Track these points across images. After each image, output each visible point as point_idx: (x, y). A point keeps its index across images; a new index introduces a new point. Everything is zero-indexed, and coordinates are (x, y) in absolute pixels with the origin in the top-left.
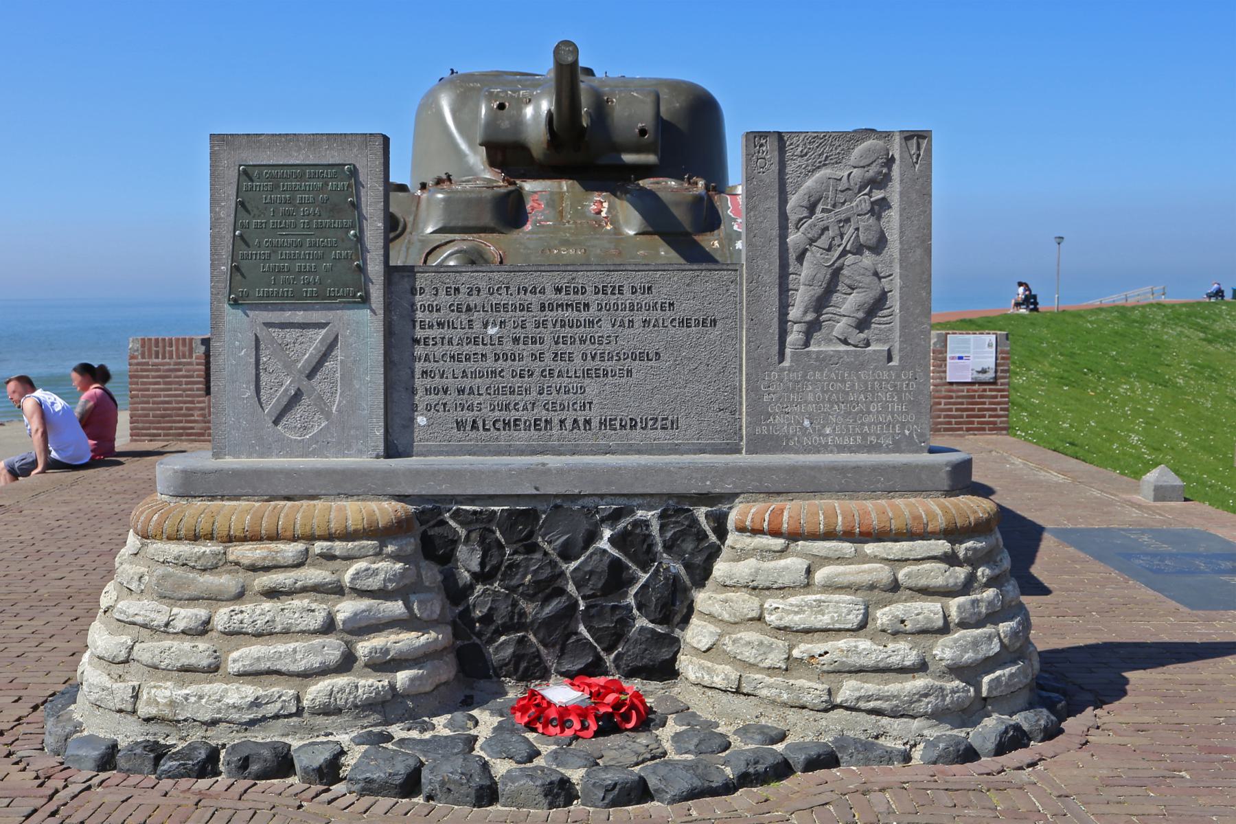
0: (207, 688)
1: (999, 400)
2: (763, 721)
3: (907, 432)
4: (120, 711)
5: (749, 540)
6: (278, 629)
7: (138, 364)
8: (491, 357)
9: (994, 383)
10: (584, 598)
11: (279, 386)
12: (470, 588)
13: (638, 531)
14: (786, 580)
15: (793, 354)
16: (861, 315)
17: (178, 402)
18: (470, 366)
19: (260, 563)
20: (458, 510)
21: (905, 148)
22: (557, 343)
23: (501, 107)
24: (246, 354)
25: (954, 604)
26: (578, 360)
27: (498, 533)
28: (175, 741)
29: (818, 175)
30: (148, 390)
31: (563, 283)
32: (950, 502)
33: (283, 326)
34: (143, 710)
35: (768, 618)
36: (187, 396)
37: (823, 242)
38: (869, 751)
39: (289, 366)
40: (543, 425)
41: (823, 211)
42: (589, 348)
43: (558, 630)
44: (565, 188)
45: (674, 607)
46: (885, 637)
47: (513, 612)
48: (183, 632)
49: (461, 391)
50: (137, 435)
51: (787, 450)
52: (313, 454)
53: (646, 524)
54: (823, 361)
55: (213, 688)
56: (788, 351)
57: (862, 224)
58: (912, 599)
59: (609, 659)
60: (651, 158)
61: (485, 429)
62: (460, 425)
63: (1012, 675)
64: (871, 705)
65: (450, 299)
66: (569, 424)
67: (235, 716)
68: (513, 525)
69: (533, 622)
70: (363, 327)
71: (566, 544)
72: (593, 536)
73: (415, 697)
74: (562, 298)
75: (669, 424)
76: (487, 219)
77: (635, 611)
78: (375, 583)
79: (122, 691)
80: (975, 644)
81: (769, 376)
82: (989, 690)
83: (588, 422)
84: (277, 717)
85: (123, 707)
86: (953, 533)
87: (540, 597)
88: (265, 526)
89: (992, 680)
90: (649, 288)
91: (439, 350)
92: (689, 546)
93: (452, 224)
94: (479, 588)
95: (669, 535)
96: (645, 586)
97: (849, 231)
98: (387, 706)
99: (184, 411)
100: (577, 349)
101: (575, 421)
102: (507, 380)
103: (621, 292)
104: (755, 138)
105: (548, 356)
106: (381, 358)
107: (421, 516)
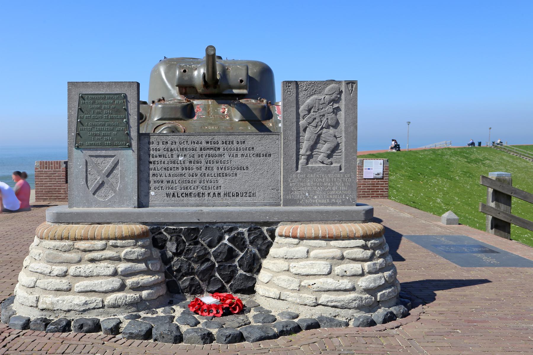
2: (289, 310)
4: (31, 306)
8: (180, 168)
9: (383, 179)
11: (95, 179)
13: (239, 236)
15: (302, 168)
16: (329, 152)
18: (172, 172)
19: (87, 249)
22: (207, 163)
23: (185, 71)
24: (82, 167)
25: (366, 265)
26: (215, 170)
27: (183, 237)
28: (53, 318)
29: (312, 98)
33: (97, 156)
34: (41, 306)
35: (291, 270)
37: (314, 124)
38: (332, 322)
39: (99, 172)
40: (201, 195)
41: (314, 112)
42: (220, 165)
45: (254, 266)
46: (338, 277)
48: (57, 276)
49: (168, 182)
52: (109, 206)
53: (242, 233)
54: (314, 170)
56: (300, 166)
57: (329, 117)
59: (228, 286)
60: (245, 91)
63: (389, 292)
64: (333, 304)
65: (164, 146)
66: (211, 194)
68: (189, 234)
69: (197, 272)
72: (221, 238)
73: (150, 301)
74: (209, 145)
75: (252, 195)
76: (179, 115)
77: (238, 267)
78: (133, 257)
79: (32, 299)
80: (375, 280)
82: (380, 298)
83: (219, 194)
84: (94, 308)
85: (32, 305)
86: (366, 237)
88: (90, 235)
89: (381, 294)
90: (244, 142)
91: (159, 166)
92: (260, 242)
93: (165, 117)
94: (176, 258)
95: (252, 238)
96: (242, 258)
97: (324, 120)
98: (138, 304)
100: (215, 166)
101: (214, 193)
102: (187, 178)
103: (232, 143)
104: (287, 83)
105: (203, 168)
106: (136, 169)
107: (152, 231)
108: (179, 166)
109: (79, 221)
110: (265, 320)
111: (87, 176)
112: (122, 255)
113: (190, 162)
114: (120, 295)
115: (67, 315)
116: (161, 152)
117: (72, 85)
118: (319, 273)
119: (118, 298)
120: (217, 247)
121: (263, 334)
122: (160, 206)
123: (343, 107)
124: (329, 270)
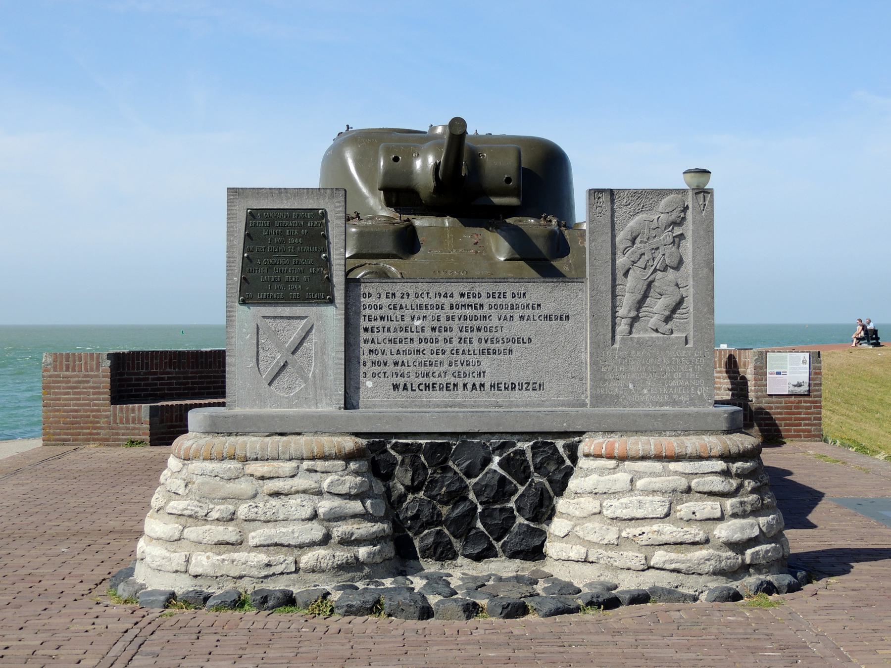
0: (236, 556)
1: (812, 410)
2: (602, 579)
3: (699, 393)
4: (177, 571)
5: (592, 462)
6: (281, 517)
7: (50, 376)
8: (416, 340)
9: (808, 395)
10: (481, 503)
11: (273, 358)
12: (402, 498)
13: (518, 457)
14: (618, 487)
15: (622, 339)
16: (667, 313)
17: (87, 411)
18: (402, 347)
19: (267, 475)
20: (396, 442)
21: (695, 200)
22: (461, 331)
23: (396, 159)
24: (250, 337)
25: (729, 503)
26: (476, 344)
27: (423, 458)
28: (214, 590)
29: (637, 218)
30: (59, 399)
31: (466, 291)
32: (725, 438)
33: (275, 318)
34: (193, 570)
35: (605, 512)
36: (95, 405)
37: (641, 263)
38: (671, 595)
39: (279, 346)
40: (452, 387)
41: (641, 242)
42: (483, 335)
43: (463, 526)
44: (447, 224)
45: (543, 510)
46: (682, 524)
47: (433, 513)
48: (217, 519)
49: (396, 364)
50: (49, 440)
51: (616, 404)
52: (296, 406)
53: (522, 452)
54: (641, 343)
55: (240, 556)
56: (618, 337)
57: (667, 252)
58: (701, 499)
59: (498, 545)
60: (513, 201)
61: (412, 390)
62: (396, 387)
63: (767, 551)
64: (673, 566)
65: (389, 301)
66: (469, 386)
67: (255, 572)
68: (434, 453)
69: (446, 520)
70: (329, 319)
71: (469, 466)
72: (487, 461)
73: (372, 565)
74: (465, 300)
75: (537, 387)
76: (389, 248)
77: (516, 513)
78: (344, 490)
79: (178, 559)
80: (742, 529)
81: (605, 354)
82: (752, 559)
83: (482, 385)
84: (282, 573)
85: (178, 569)
86: (727, 457)
87: (450, 501)
88: (270, 452)
89: (753, 553)
90: (524, 294)
91: (381, 336)
92: (552, 468)
93: (364, 252)
94: (410, 497)
95: (538, 460)
96: (522, 495)
97: (659, 256)
98: (353, 566)
99: (91, 419)
100: (475, 335)
101: (474, 385)
102: (428, 357)
103: (504, 297)
104: (595, 194)
105: (455, 340)
106: (343, 341)
107: (370, 446)
108: (415, 335)
109: (248, 430)
110: (564, 591)
111: (258, 352)
112: (325, 485)
113: (433, 329)
114: (321, 552)
115: (237, 585)
116: (384, 312)
117: (234, 193)
118: (651, 516)
119: (321, 557)
120: (480, 476)
121: (560, 605)
122: (382, 406)
123: (689, 235)
124: (666, 510)
